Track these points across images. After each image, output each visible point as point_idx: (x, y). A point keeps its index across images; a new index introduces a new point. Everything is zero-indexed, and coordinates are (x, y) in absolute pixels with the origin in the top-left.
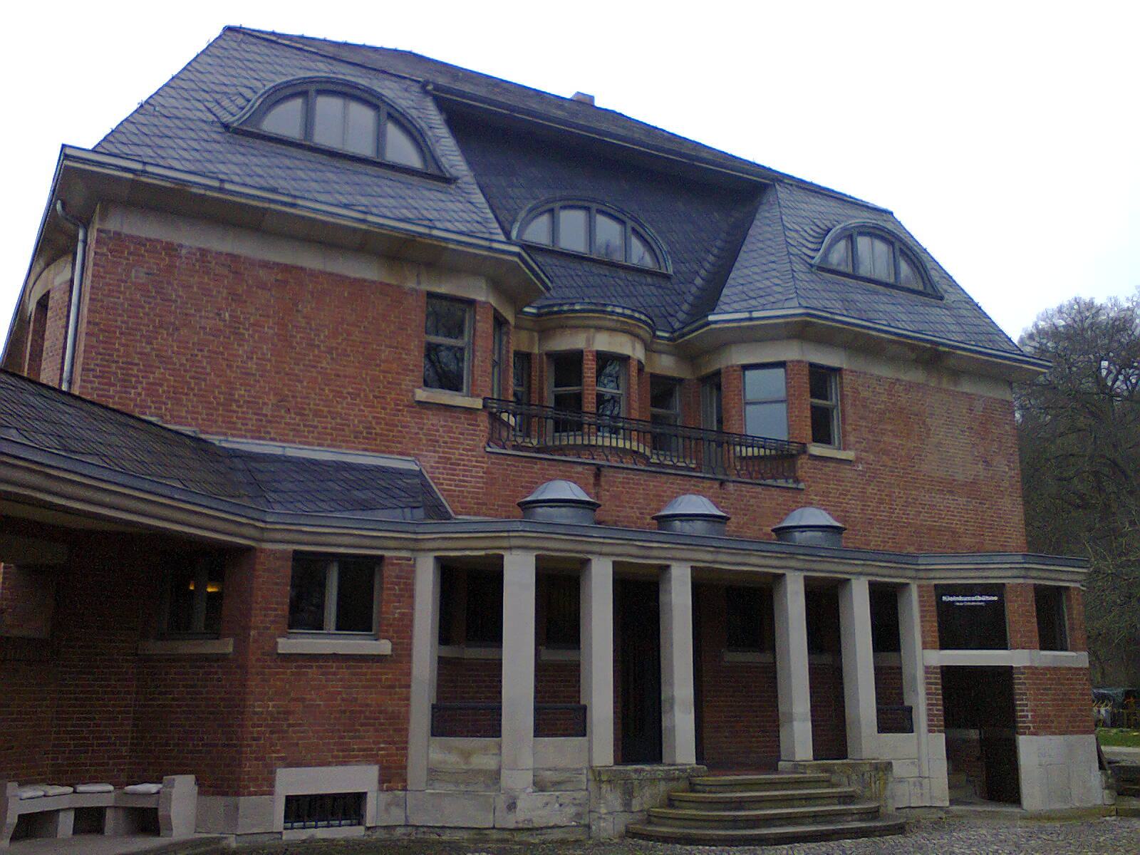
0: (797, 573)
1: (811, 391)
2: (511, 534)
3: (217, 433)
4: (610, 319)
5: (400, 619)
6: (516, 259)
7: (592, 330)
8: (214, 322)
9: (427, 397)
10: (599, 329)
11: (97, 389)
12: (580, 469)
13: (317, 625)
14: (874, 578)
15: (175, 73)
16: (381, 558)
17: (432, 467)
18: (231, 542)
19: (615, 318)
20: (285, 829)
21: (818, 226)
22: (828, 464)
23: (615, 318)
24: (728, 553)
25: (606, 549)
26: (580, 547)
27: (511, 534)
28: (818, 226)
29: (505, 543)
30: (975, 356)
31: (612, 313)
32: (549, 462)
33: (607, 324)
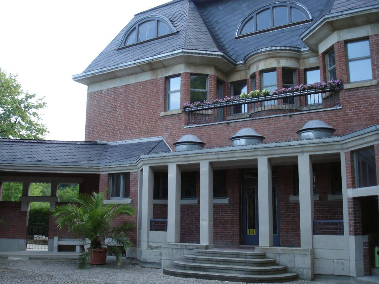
0: (264, 157)
1: (191, 86)
2: (170, 157)
3: (111, 141)
4: (261, 55)
5: (135, 192)
6: (183, 54)
7: (258, 62)
8: (22, 122)
9: (164, 114)
10: (260, 61)
11: (362, 94)
12: (220, 126)
13: (118, 195)
14: (311, 153)
15: (123, 28)
16: (129, 173)
17: (167, 138)
18: (326, 154)
19: (263, 54)
20: (125, 256)
21: (175, 18)
22: (360, 91)
23: (263, 54)
24: (251, 151)
25: (171, 160)
26: (163, 161)
27: (170, 157)
28: (175, 18)
29: (201, 158)
30: (310, 34)
31: (261, 52)
32: (208, 126)
33: (261, 57)
